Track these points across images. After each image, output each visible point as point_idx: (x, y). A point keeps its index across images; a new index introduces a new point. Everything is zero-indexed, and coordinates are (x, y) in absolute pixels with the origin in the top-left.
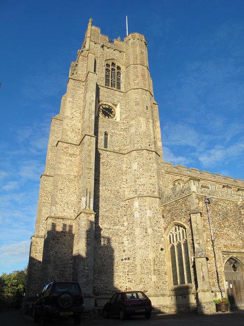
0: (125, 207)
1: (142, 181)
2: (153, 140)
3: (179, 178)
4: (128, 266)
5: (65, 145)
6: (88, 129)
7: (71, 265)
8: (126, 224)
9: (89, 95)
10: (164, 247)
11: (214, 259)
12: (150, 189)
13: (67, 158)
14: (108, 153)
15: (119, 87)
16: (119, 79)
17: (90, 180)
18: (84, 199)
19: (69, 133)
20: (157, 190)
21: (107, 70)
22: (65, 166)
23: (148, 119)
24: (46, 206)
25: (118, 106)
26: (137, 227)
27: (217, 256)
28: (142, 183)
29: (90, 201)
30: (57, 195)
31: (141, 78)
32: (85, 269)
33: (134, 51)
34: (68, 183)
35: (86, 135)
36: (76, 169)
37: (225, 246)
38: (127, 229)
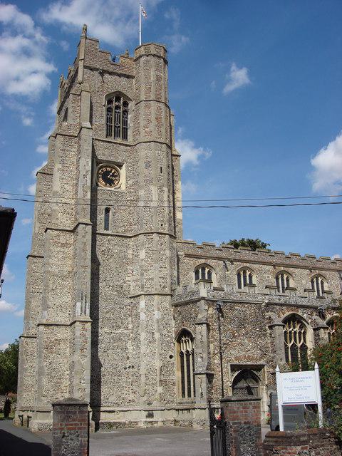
1: (151, 274)
3: (203, 261)
4: (133, 375)
5: (56, 233)
7: (68, 376)
8: (130, 326)
9: (82, 162)
12: (159, 284)
13: (59, 249)
15: (125, 137)
16: (125, 123)
18: (79, 304)
21: (109, 110)
23: (161, 187)
24: (34, 296)
31: (154, 122)
35: (79, 223)
37: (237, 358)
38: (132, 333)
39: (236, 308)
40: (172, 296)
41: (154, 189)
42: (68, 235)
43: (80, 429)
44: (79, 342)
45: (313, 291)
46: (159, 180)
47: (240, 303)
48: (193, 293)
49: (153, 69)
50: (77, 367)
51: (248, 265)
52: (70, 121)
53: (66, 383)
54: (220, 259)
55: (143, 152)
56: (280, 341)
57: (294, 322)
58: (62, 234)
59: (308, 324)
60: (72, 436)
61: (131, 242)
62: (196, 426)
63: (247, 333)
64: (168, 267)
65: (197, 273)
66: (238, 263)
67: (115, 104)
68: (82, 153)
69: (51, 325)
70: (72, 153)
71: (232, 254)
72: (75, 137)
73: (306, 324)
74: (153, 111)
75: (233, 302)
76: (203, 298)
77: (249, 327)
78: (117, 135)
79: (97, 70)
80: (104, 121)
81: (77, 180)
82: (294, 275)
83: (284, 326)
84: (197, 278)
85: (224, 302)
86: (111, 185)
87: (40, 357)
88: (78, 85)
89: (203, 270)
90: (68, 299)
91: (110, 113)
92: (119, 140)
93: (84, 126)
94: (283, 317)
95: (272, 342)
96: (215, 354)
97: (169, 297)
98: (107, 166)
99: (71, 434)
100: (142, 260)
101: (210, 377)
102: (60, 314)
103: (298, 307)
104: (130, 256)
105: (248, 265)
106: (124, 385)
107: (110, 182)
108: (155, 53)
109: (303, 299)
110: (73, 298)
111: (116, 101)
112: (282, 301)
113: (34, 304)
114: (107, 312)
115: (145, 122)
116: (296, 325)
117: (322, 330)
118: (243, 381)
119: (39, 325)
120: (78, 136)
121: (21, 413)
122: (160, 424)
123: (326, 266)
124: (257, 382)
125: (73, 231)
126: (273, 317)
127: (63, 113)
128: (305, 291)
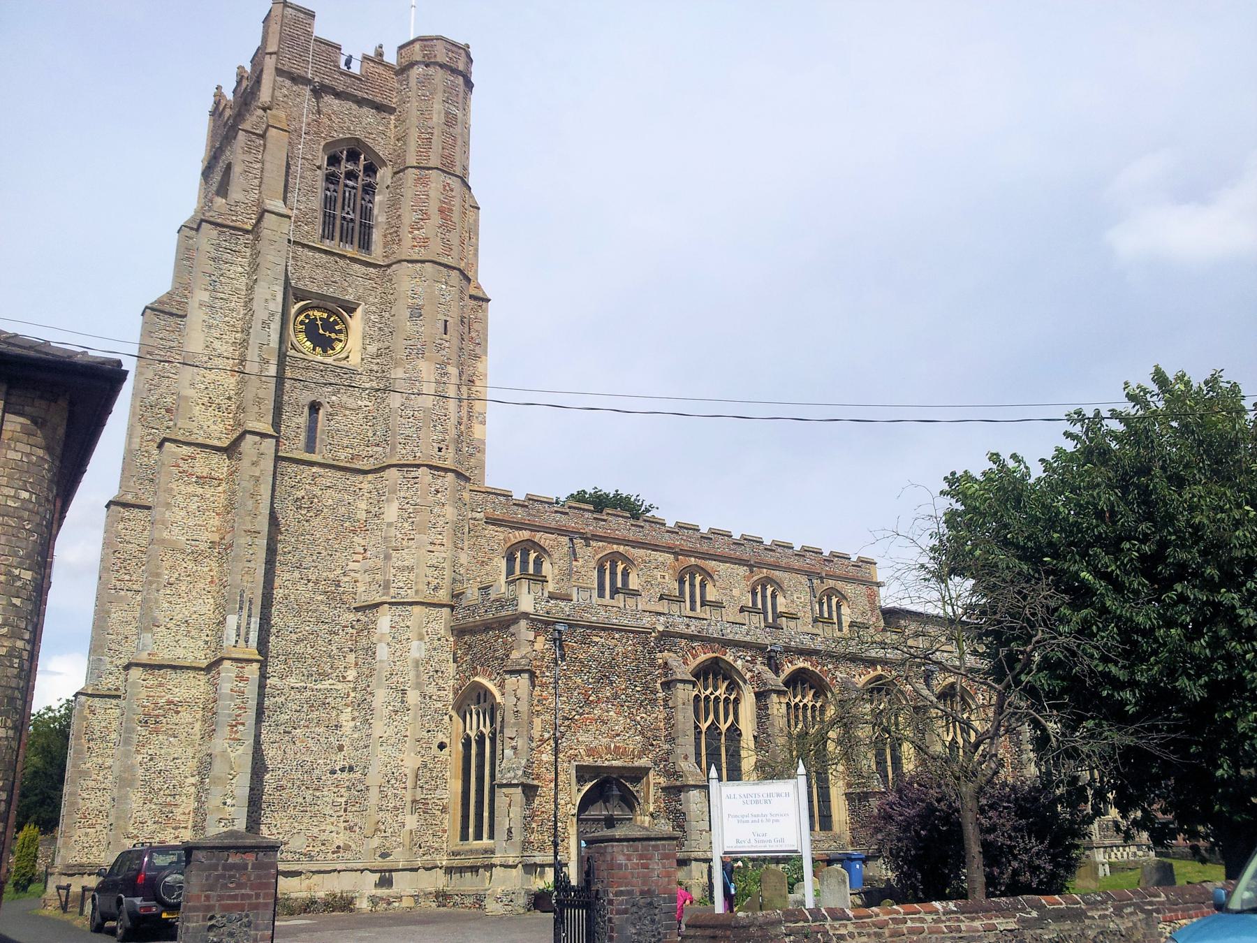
0: (352, 627)
2: (453, 433)
3: (525, 535)
4: (349, 789)
5: (186, 450)
6: (256, 409)
7: (193, 789)
8: (351, 674)
9: (261, 291)
10: (447, 741)
11: (553, 785)
13: (190, 489)
14: (314, 469)
15: (365, 244)
16: (366, 213)
17: (252, 565)
18: (232, 620)
19: (197, 410)
20: (447, 582)
21: (331, 178)
22: (183, 513)
23: (443, 365)
24: (122, 599)
25: (359, 310)
26: (378, 687)
27: (562, 777)
28: (406, 563)
29: (248, 624)
30: (157, 601)
31: (436, 219)
32: (225, 804)
33: (424, 113)
34: (191, 565)
35: (246, 432)
36: (216, 521)
37: (591, 752)
38: (354, 689)
39: (596, 639)
40: (452, 608)
41: (426, 370)
42: (216, 458)
43: (256, 907)
44: (227, 708)
45: (680, 599)
46: (440, 348)
47: (604, 629)
48: (501, 603)
49: (439, 97)
50: (218, 768)
51: (621, 549)
52: (236, 194)
53: (187, 804)
54: (561, 531)
55: (406, 281)
56: (685, 717)
57: (715, 677)
58: (201, 455)
59: (745, 682)
60: (234, 927)
61: (366, 483)
62: (492, 907)
63: (616, 696)
64: (449, 545)
65: (510, 559)
66: (601, 544)
67: (346, 166)
68: (263, 271)
69: (160, 667)
70: (237, 268)
71: (585, 522)
72: (247, 232)
73: (741, 683)
74: (432, 194)
75: (589, 627)
76: (525, 615)
77: (621, 683)
78: (346, 237)
79: (307, 82)
80: (316, 203)
81: (246, 331)
82: (716, 577)
83: (694, 685)
84: (510, 571)
85: (570, 626)
86: (325, 351)
87: (127, 742)
88: (260, 112)
89: (525, 554)
90: (206, 607)
91: (332, 187)
92: (350, 251)
93: (269, 207)
94: (693, 663)
95: (668, 719)
96: (543, 741)
97: (446, 611)
98: (318, 308)
99: (230, 921)
100: (390, 525)
101: (530, 791)
102: (185, 642)
103: (727, 644)
104: (362, 515)
105: (621, 549)
106: (328, 811)
107: (324, 344)
108: (445, 60)
109: (736, 628)
110: (217, 606)
111: (348, 160)
112: (692, 630)
113: (115, 616)
114: (299, 641)
115: (415, 217)
116: (720, 682)
117: (774, 697)
118: (600, 804)
119: (127, 667)
120: (255, 231)
121: (65, 881)
122: (407, 903)
123: (783, 562)
124: (632, 808)
125: (231, 450)
126: (671, 662)
127: (217, 177)
128: (742, 610)
